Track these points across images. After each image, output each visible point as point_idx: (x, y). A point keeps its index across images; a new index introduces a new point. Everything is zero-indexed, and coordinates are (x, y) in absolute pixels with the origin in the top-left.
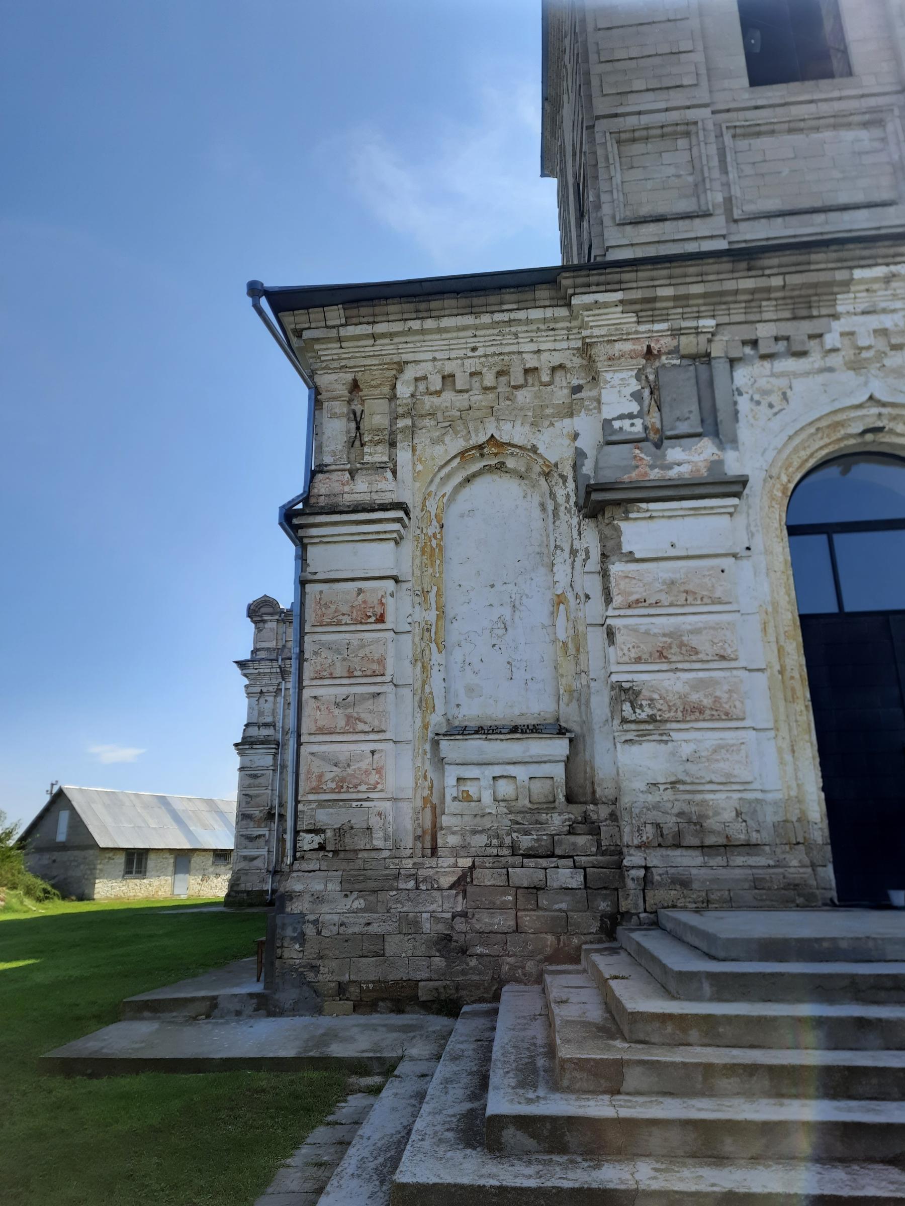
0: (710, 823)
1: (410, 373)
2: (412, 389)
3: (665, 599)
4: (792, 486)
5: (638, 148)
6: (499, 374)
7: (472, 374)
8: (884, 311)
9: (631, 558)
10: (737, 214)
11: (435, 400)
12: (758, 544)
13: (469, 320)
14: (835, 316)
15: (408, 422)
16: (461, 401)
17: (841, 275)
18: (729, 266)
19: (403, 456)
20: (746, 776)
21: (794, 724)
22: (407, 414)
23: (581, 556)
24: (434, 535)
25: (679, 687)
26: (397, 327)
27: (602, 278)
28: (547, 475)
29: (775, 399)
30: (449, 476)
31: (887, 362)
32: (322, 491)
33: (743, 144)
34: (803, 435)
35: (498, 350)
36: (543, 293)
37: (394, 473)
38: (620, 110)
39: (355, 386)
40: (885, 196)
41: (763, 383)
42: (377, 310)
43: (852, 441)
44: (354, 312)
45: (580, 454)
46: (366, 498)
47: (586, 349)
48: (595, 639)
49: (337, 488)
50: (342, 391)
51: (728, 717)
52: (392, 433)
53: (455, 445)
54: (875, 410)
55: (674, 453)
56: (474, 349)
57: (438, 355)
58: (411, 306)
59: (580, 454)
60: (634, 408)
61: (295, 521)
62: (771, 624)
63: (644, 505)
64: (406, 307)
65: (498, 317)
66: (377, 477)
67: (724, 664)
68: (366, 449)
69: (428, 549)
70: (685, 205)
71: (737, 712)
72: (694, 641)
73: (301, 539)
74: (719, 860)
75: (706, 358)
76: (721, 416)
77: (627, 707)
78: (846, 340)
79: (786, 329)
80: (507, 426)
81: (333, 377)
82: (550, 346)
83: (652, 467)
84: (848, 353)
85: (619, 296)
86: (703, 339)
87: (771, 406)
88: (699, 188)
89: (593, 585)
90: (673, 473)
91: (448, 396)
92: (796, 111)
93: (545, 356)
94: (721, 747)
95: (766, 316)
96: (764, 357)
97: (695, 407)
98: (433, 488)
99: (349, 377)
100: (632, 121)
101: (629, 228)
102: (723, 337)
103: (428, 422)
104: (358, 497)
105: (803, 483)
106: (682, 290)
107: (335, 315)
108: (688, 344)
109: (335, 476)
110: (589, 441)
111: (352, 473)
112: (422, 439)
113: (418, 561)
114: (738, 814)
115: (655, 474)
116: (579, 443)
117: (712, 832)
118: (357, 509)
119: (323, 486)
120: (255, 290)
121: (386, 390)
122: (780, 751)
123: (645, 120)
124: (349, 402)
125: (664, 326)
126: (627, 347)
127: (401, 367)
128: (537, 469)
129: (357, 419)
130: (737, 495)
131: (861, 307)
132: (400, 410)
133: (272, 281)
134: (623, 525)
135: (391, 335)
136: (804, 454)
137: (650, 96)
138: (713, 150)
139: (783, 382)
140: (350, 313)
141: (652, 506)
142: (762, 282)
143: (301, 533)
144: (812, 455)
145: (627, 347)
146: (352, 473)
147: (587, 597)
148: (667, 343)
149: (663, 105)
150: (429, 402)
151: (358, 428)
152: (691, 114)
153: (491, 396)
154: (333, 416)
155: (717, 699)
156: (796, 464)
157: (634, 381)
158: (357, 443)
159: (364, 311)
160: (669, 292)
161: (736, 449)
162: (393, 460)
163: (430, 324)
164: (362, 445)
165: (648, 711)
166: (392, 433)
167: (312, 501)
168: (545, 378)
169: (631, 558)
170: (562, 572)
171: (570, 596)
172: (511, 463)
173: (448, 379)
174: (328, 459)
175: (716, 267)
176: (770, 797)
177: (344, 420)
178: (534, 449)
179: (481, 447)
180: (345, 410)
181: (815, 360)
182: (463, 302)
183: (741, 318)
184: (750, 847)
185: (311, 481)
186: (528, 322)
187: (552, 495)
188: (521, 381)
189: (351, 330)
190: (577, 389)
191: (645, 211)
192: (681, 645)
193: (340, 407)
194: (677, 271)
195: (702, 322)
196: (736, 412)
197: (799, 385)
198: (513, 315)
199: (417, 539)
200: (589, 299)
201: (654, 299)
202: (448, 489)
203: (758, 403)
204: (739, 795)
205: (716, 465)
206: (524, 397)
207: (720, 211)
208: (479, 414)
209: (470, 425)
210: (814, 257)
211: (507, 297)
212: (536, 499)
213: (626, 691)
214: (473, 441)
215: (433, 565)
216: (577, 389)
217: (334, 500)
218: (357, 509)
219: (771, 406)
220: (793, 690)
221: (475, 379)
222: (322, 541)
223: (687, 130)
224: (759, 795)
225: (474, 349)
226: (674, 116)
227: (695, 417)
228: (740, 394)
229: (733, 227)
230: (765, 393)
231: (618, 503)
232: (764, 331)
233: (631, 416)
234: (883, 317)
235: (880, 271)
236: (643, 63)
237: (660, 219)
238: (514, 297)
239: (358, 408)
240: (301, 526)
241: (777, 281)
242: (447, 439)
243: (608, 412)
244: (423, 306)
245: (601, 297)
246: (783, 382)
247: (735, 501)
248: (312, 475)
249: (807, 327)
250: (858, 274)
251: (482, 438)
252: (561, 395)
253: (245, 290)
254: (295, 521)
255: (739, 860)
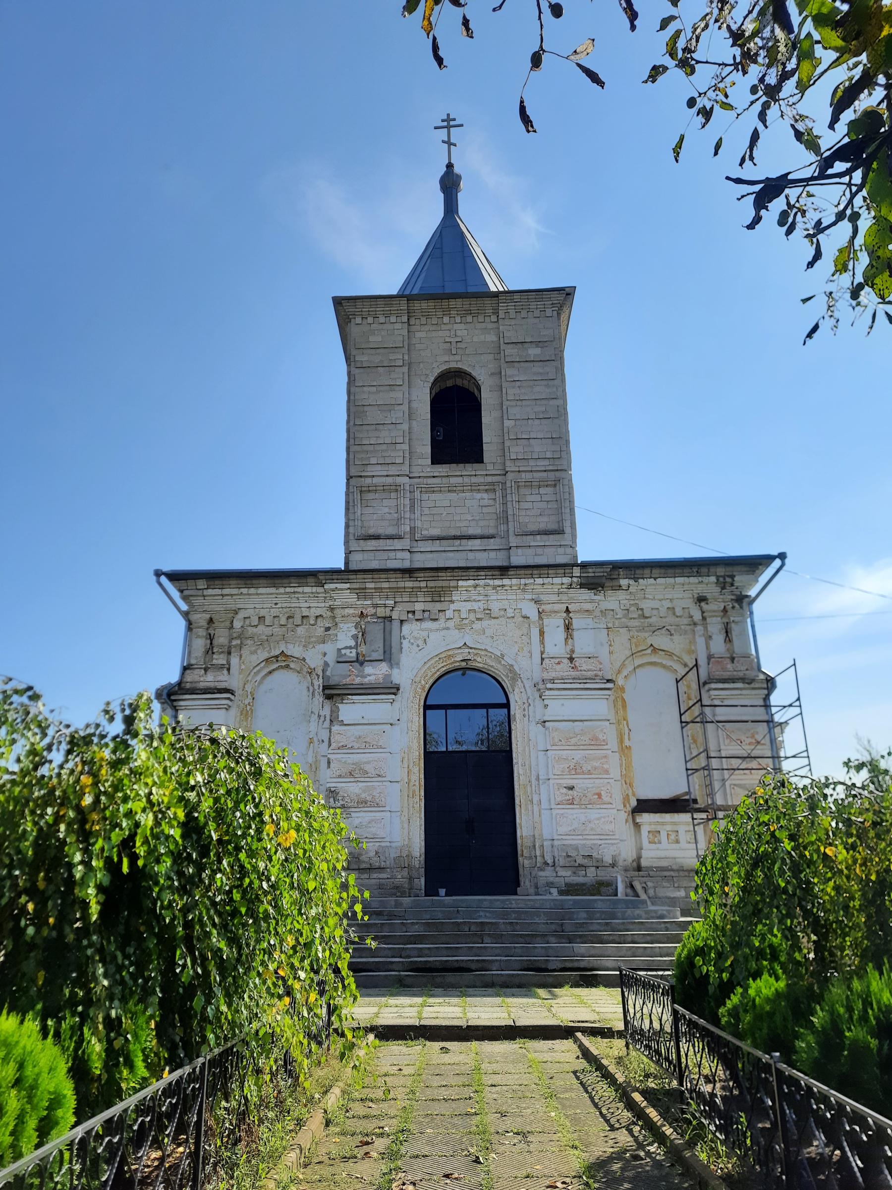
0: (363, 858)
1: (241, 615)
2: (241, 624)
3: (356, 745)
4: (428, 686)
5: (371, 496)
6: (289, 618)
7: (274, 617)
8: (475, 601)
9: (342, 723)
10: (417, 536)
11: (254, 629)
12: (404, 718)
13: (273, 590)
14: (452, 602)
15: (238, 642)
16: (268, 631)
17: (453, 583)
18: (400, 575)
19: (235, 661)
20: (382, 834)
21: (411, 809)
22: (239, 637)
23: (322, 719)
24: (249, 704)
25: (357, 791)
26: (235, 591)
27: (339, 577)
28: (310, 673)
29: (420, 642)
30: (259, 671)
31: (474, 626)
32: (189, 680)
33: (425, 496)
34: (433, 661)
35: (289, 605)
36: (311, 580)
37: (229, 670)
38: (363, 474)
39: (211, 621)
40: (492, 531)
41: (415, 634)
42: (224, 582)
43: (458, 664)
44: (212, 583)
45: (326, 664)
46: (212, 685)
47: (397, 525)
48: (324, 763)
49: (197, 678)
50: (204, 623)
51: (378, 805)
52: (230, 647)
53: (263, 655)
54: (467, 650)
55: (368, 669)
56: (276, 604)
57: (257, 606)
58: (243, 582)
59: (326, 664)
60: (353, 643)
61: (173, 698)
62: (406, 759)
63: (350, 697)
64: (239, 582)
65: (288, 590)
66: (219, 673)
67: (380, 779)
68: (215, 656)
69: (244, 712)
70: (391, 531)
71: (381, 803)
72: (367, 767)
73: (175, 707)
74: (366, 876)
75: (389, 619)
76: (393, 650)
77: (332, 800)
78: (456, 614)
79: (429, 606)
80: (290, 646)
81: (199, 616)
82: (316, 605)
83: (357, 676)
84: (457, 620)
85: (348, 586)
86: (388, 609)
87: (418, 646)
88: (398, 522)
89: (324, 735)
90: (366, 680)
91: (261, 628)
92: (453, 480)
93: (312, 610)
94: (373, 820)
95: (419, 599)
96: (417, 620)
97: (381, 645)
98: (250, 678)
99: (208, 616)
100: (369, 480)
101: (362, 541)
102: (399, 608)
103: (249, 642)
104: (208, 684)
105: (446, 677)
106: (379, 585)
107: (202, 584)
108: (381, 612)
109: (196, 672)
110: (331, 658)
111: (206, 670)
112: (245, 652)
113: (238, 719)
114: (376, 853)
115: (358, 680)
116: (326, 659)
117: (364, 862)
118: (207, 691)
119: (190, 677)
120: (158, 574)
121: (228, 624)
122: (402, 822)
123: (375, 480)
124: (207, 629)
125: (369, 602)
126: (351, 611)
127: (236, 612)
128: (305, 670)
129: (211, 638)
130: (395, 694)
131: (464, 598)
132: (235, 635)
133: (166, 568)
134: (340, 706)
135: (232, 595)
136: (433, 670)
137: (379, 467)
138: (407, 502)
139: (425, 634)
140: (209, 583)
141: (354, 697)
142: (416, 584)
143: (175, 704)
144: (438, 670)
145: (351, 611)
146: (206, 670)
147: (323, 741)
148: (371, 611)
149: (385, 473)
150: (251, 630)
151: (211, 644)
152: (399, 480)
153: (284, 629)
154: (198, 637)
155: (373, 797)
156: (430, 674)
157: (353, 629)
158: (210, 652)
159: (217, 582)
160: (372, 585)
161: (399, 668)
162: (229, 663)
163: (252, 591)
164: (213, 653)
165: (341, 802)
166: (230, 647)
167: (183, 685)
168: (312, 622)
169: (342, 723)
170: (313, 726)
171: (315, 739)
172: (292, 665)
173: (261, 619)
174: (193, 661)
175: (394, 576)
176: (394, 845)
177: (204, 639)
178: (304, 660)
179: (277, 657)
180: (205, 634)
181: (441, 623)
182: (270, 581)
183: (407, 599)
184: (381, 869)
185: (183, 674)
186: (303, 593)
187: (313, 685)
188: (300, 623)
189: (210, 592)
190: (328, 629)
191: (372, 531)
192: (361, 769)
193: (202, 632)
194: (376, 576)
195: (387, 602)
196: (402, 648)
197: (433, 635)
198: (296, 589)
199: (238, 706)
200: (332, 586)
201: (365, 588)
202: (258, 678)
203: (412, 644)
204: (378, 844)
205: (387, 676)
206: (301, 630)
207: (408, 536)
208: (277, 638)
209: (272, 645)
210: (440, 574)
211: (293, 581)
212: (305, 684)
213: (332, 792)
214: (272, 654)
215: (247, 720)
216: (328, 629)
217: (194, 685)
218: (207, 691)
219: (418, 646)
220: (414, 791)
221: (276, 619)
222: (186, 708)
223: (396, 488)
224: (388, 844)
225: (276, 604)
226: (389, 480)
227: (381, 650)
228: (404, 639)
229: (415, 544)
230: (416, 638)
231: (339, 695)
232: (419, 607)
233: (350, 648)
234: (474, 603)
235: (471, 582)
236: (378, 448)
237: (377, 537)
238: (297, 581)
239: (212, 632)
240: (175, 700)
241: (423, 584)
242: (259, 651)
243: (341, 645)
244: (248, 582)
245: (338, 586)
246: (425, 634)
247: (393, 696)
248: (185, 669)
249: (438, 606)
250: (461, 583)
251: (277, 653)
252: (319, 631)
253: (152, 573)
254: (173, 698)
255: (375, 876)
